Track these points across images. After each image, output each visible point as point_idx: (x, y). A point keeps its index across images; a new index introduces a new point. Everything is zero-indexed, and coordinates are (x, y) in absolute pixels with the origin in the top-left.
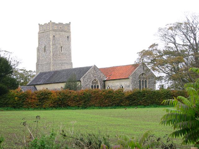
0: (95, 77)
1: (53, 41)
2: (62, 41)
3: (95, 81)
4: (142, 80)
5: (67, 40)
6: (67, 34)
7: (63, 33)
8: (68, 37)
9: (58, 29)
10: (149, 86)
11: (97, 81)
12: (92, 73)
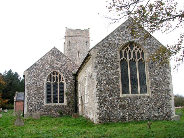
0: (54, 68)
1: (69, 46)
2: (79, 46)
3: (55, 76)
4: (137, 60)
5: (85, 45)
6: (85, 40)
7: (81, 38)
8: (86, 42)
9: (74, 35)
10: (150, 74)
11: (60, 76)
12: (48, 62)
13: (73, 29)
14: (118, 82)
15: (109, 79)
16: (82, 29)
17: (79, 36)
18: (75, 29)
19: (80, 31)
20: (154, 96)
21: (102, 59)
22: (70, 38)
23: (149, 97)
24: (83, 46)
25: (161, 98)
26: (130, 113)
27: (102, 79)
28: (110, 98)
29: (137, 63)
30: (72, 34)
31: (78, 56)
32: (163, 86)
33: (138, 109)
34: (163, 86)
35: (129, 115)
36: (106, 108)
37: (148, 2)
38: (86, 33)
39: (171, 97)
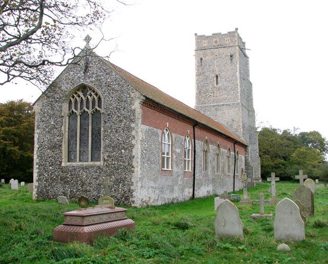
5: (230, 61)
7: (221, 50)
8: (231, 56)
13: (207, 35)
14: (61, 146)
15: (51, 142)
16: (224, 32)
17: (218, 46)
18: (211, 35)
19: (220, 37)
20: (106, 165)
21: (46, 115)
22: (201, 52)
23: (99, 167)
24: (226, 63)
25: (118, 169)
26: (72, 189)
27: (44, 141)
28: (51, 168)
29: (90, 116)
30: (205, 44)
31: (217, 84)
32: (123, 151)
33: (83, 185)
34: (123, 151)
35: (71, 192)
36: (45, 181)
37: (49, 16)
38: (231, 39)
39: (133, 167)
